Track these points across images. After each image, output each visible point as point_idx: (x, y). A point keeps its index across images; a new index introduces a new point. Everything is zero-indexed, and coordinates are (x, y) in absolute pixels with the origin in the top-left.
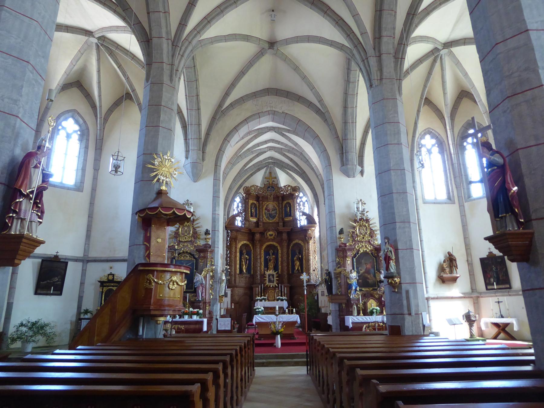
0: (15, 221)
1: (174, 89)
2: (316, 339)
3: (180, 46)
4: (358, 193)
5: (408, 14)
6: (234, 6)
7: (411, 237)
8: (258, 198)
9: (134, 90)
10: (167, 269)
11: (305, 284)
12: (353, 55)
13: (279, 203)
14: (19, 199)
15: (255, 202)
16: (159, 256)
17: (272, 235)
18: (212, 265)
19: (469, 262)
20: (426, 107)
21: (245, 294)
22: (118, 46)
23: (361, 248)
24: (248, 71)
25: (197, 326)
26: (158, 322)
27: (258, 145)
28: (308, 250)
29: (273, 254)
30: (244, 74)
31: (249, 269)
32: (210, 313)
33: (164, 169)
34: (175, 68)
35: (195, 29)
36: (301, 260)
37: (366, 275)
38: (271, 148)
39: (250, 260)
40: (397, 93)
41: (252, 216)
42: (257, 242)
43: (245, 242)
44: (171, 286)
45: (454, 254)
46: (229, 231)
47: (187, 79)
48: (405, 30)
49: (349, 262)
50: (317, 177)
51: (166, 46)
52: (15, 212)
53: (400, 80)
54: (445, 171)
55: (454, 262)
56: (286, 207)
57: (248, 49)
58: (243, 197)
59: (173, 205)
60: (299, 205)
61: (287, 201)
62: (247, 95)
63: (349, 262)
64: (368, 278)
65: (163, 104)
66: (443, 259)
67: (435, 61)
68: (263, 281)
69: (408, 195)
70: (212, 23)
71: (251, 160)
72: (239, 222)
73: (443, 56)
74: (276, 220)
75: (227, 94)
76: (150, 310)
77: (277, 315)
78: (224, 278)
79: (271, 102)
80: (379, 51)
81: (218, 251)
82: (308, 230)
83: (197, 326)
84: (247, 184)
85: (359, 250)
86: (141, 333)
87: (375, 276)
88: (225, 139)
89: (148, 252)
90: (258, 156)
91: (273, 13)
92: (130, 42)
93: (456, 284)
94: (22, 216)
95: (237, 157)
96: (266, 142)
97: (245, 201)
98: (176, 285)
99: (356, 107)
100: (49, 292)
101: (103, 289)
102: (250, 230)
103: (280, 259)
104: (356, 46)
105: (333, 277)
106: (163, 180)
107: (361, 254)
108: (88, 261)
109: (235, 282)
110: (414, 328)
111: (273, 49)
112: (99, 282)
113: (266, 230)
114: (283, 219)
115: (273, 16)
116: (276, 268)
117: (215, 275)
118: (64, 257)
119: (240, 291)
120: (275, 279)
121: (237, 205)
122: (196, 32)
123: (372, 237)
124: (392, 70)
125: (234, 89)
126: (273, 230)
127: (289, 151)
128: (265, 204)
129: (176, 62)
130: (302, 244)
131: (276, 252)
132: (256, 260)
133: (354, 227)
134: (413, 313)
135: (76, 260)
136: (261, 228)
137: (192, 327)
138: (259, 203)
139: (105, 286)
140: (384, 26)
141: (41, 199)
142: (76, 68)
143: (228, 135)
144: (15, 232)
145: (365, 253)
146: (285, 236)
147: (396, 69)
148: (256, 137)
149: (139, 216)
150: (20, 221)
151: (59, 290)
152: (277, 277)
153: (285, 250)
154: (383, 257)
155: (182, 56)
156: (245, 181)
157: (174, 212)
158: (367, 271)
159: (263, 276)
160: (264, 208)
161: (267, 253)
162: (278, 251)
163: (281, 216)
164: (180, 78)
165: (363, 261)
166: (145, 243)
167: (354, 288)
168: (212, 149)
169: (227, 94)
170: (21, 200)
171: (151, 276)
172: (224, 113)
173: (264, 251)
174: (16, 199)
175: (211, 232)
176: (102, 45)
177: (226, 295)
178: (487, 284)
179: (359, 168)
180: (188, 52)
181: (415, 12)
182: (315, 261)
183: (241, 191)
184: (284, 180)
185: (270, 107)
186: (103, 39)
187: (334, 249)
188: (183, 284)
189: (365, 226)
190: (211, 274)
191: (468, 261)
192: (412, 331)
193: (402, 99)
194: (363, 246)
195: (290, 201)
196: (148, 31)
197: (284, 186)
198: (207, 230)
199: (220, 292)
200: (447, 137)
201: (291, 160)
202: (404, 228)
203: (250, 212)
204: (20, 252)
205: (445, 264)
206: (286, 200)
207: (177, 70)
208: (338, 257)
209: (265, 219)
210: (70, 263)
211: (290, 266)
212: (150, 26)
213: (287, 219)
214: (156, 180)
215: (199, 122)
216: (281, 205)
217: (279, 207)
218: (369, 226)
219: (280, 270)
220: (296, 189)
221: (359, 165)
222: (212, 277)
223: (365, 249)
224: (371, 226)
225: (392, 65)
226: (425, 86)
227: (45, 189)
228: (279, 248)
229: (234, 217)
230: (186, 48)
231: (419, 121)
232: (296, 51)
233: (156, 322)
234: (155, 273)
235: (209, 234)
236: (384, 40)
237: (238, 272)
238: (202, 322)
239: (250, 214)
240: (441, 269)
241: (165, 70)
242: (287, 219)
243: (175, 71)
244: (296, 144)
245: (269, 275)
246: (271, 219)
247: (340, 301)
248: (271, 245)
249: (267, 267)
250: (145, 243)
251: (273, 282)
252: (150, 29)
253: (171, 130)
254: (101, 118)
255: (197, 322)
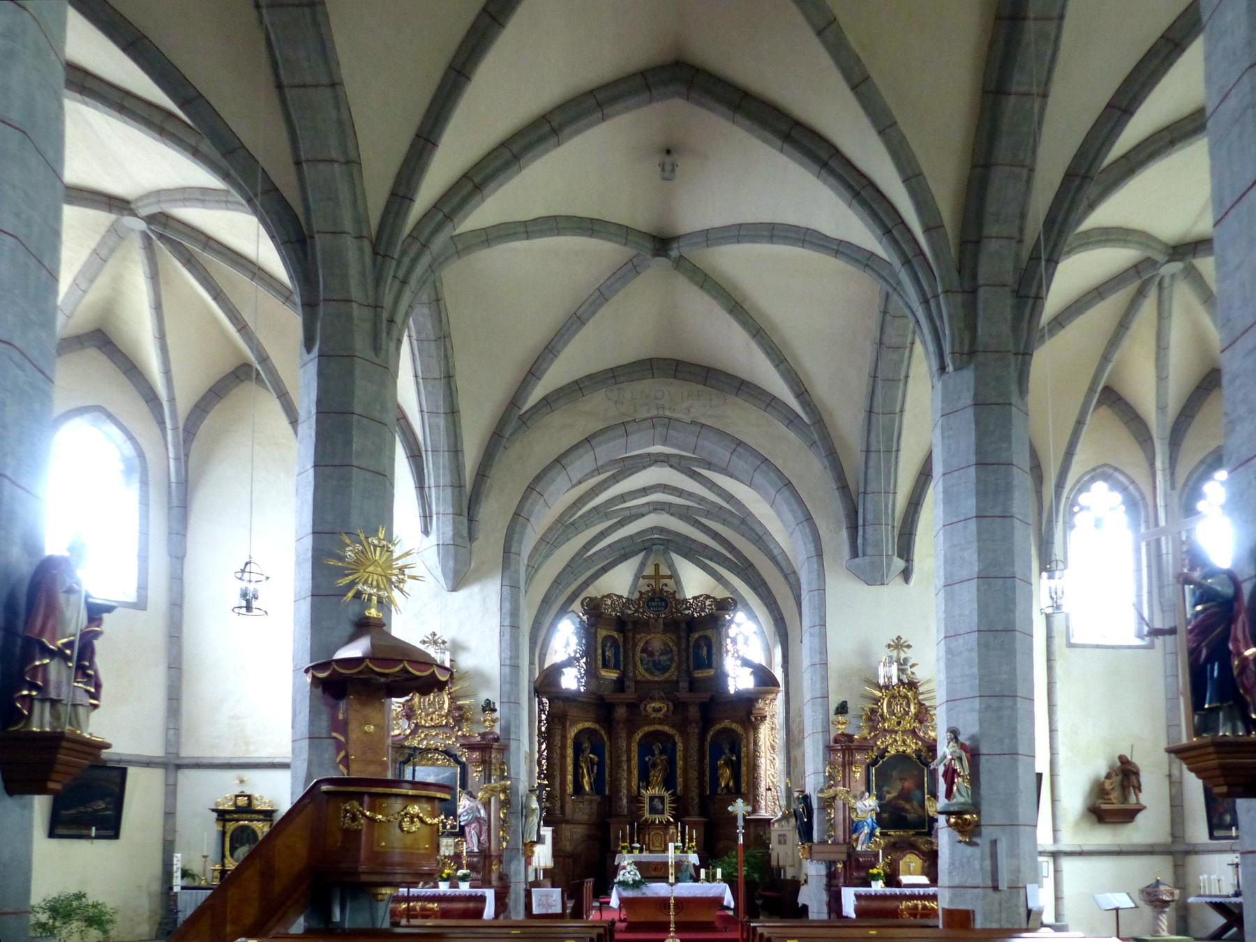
0: (37, 706)
1: (388, 372)
2: (762, 935)
3: (396, 256)
4: (893, 626)
5: (1069, 175)
6: (553, 141)
7: (1015, 728)
8: (621, 624)
9: (264, 359)
10: (394, 791)
11: (740, 823)
12: (899, 283)
13: (679, 638)
14: (40, 659)
15: (615, 634)
16: (371, 762)
17: (659, 710)
18: (503, 778)
19: (1174, 779)
20: (1105, 411)
21: (589, 837)
22: (208, 241)
23: (891, 745)
24: (594, 313)
25: (471, 905)
26: (380, 897)
27: (623, 498)
28: (756, 743)
29: (662, 752)
30: (584, 324)
31: (598, 785)
32: (503, 878)
33: (371, 569)
34: (385, 315)
35: (436, 207)
36: (735, 768)
37: (902, 803)
38: (658, 507)
39: (601, 764)
40: (1014, 387)
41: (605, 666)
42: (621, 726)
43: (588, 725)
44: (406, 825)
45: (1137, 760)
46: (545, 700)
47: (419, 333)
48: (1047, 240)
49: (858, 775)
50: (786, 577)
51: (355, 256)
52: (33, 686)
53: (1025, 355)
54: (1139, 570)
55: (1133, 778)
56: (697, 646)
57: (590, 257)
58: (582, 620)
59: (404, 652)
60: (734, 641)
61: (701, 633)
62: (590, 377)
63: (858, 775)
64: (906, 811)
65: (358, 409)
66: (1103, 770)
67: (1141, 293)
68: (635, 814)
69: (1018, 636)
70: (486, 191)
71: (603, 535)
72: (571, 681)
73: (1167, 282)
74: (671, 674)
75: (533, 373)
76: (358, 874)
77: (672, 885)
78: (535, 805)
79: (659, 394)
80: (974, 277)
81: (518, 748)
82: (757, 700)
83: (471, 905)
84: (592, 592)
85: (885, 750)
86: (337, 916)
87: (922, 805)
88: (530, 488)
89: (342, 754)
90: (621, 524)
91: (668, 159)
92: (243, 230)
93: (1130, 826)
94: (53, 695)
95: (564, 527)
96: (645, 491)
97: (588, 633)
98: (418, 824)
99: (902, 411)
100: (85, 832)
101: (224, 826)
102: (601, 698)
103: (680, 763)
104: (907, 262)
105: (815, 805)
106: (370, 595)
107: (893, 757)
108: (179, 767)
109: (563, 812)
110: (1004, 915)
111: (666, 256)
112: (213, 810)
113: (645, 697)
114: (689, 673)
115: (668, 168)
116: (669, 783)
117: (513, 798)
118: (117, 758)
119: (574, 833)
120: (667, 806)
121: (565, 640)
122: (440, 215)
123: (921, 722)
124: (1006, 329)
125: (552, 361)
126: (661, 699)
127: (708, 514)
128: (642, 639)
129: (388, 300)
130: (740, 730)
131: (669, 746)
132: (616, 764)
133: (877, 700)
134: (1003, 885)
135: (148, 763)
136: (630, 695)
137: (460, 906)
138: (625, 637)
139: (231, 820)
140: (992, 207)
141: (91, 660)
142: (90, 298)
143: (538, 478)
144: (42, 726)
145: (902, 757)
146: (694, 712)
147: (1015, 328)
148: (615, 479)
149: (314, 677)
150: (48, 705)
151: (110, 827)
152: (672, 802)
153: (694, 744)
154: (941, 769)
155: (404, 282)
156: (586, 584)
157: (405, 670)
158: (905, 795)
159: (636, 799)
160: (639, 648)
161: (645, 748)
162: (675, 744)
163: (684, 667)
164: (399, 341)
165: (894, 773)
166: (334, 734)
167: (866, 830)
168: (494, 513)
169: (533, 373)
170: (46, 661)
171: (356, 804)
172: (526, 421)
173: (640, 744)
174: (34, 660)
175: (497, 706)
176: (161, 237)
177: (540, 840)
178: (1212, 828)
179: (899, 564)
180: (419, 270)
181: (1088, 170)
182: (770, 768)
183: (577, 606)
184: (694, 582)
185: (658, 408)
186: (163, 220)
187: (821, 747)
188: (436, 821)
189: (906, 697)
190: (502, 797)
191: (1170, 776)
192: (999, 920)
193: (1026, 405)
194: (896, 741)
195: (709, 633)
196: (299, 210)
197: (695, 598)
198: (488, 702)
199: (526, 836)
200: (1155, 488)
201: (715, 535)
202: (999, 709)
203: (600, 657)
204: (58, 767)
205: (1108, 782)
206: (698, 632)
207: (391, 321)
208: (830, 763)
209: (642, 673)
210: (132, 771)
211: (707, 779)
212: (305, 200)
213: (699, 674)
214: (350, 594)
215: (456, 446)
216: (684, 642)
217: (678, 644)
218: (916, 697)
219: (679, 788)
220: (724, 606)
221: (900, 556)
222: (505, 804)
223: (901, 749)
224: (921, 697)
225: (1008, 314)
226: (1106, 358)
227: (97, 635)
228: (678, 738)
229: (556, 670)
230: (415, 260)
231: (1079, 447)
232: (735, 262)
233: (375, 898)
234: (366, 799)
235: (494, 710)
236: (992, 246)
237: (570, 788)
238: (482, 899)
239: (600, 662)
240: (1099, 790)
241: (356, 321)
242: (699, 674)
243: (384, 325)
244: (729, 497)
245: (652, 798)
246: (657, 673)
247: (832, 857)
248: (656, 732)
249: (645, 779)
250: (334, 734)
251: (662, 813)
252: (307, 209)
253: (385, 478)
254: (175, 429)
255: (469, 898)
